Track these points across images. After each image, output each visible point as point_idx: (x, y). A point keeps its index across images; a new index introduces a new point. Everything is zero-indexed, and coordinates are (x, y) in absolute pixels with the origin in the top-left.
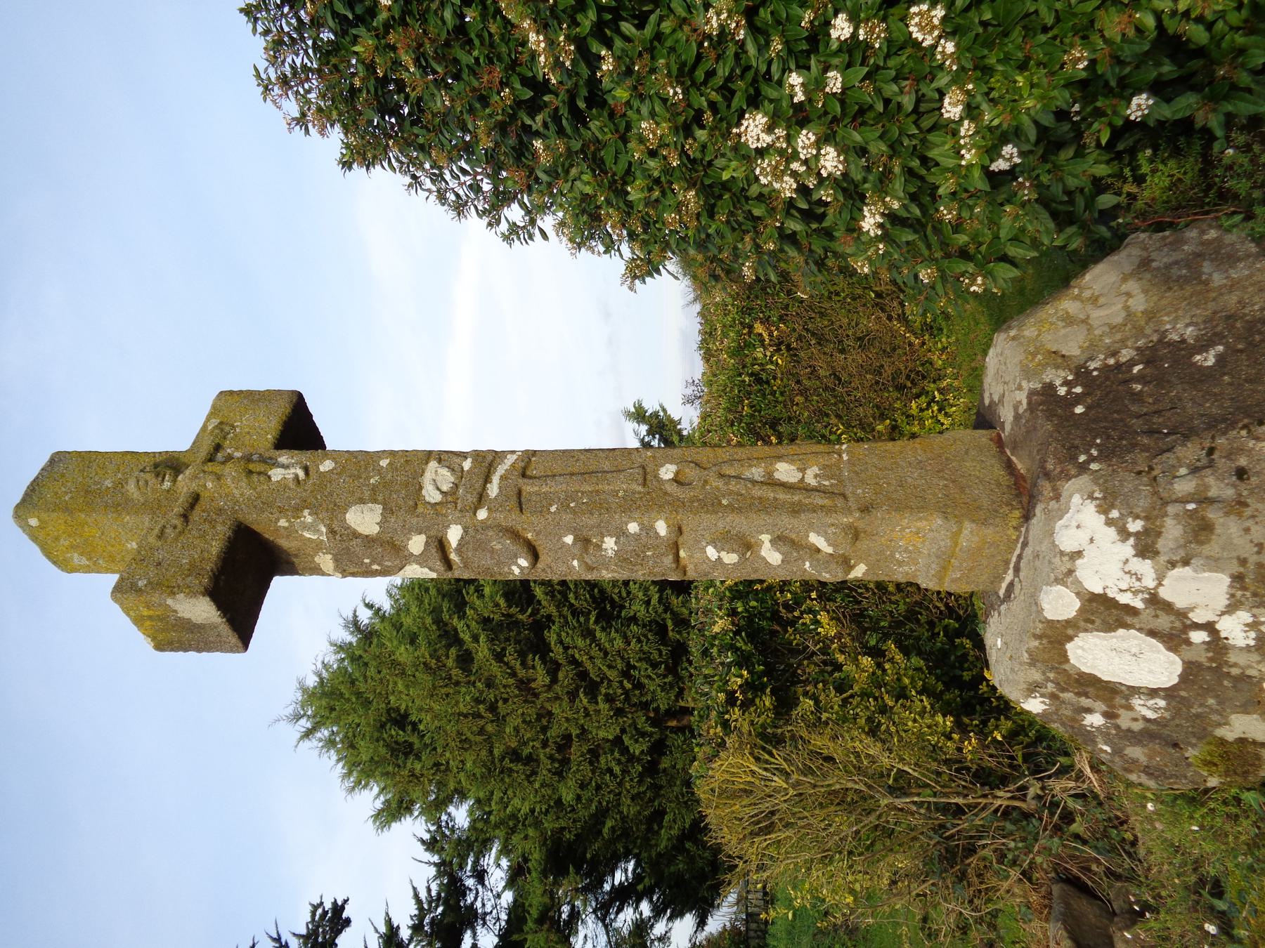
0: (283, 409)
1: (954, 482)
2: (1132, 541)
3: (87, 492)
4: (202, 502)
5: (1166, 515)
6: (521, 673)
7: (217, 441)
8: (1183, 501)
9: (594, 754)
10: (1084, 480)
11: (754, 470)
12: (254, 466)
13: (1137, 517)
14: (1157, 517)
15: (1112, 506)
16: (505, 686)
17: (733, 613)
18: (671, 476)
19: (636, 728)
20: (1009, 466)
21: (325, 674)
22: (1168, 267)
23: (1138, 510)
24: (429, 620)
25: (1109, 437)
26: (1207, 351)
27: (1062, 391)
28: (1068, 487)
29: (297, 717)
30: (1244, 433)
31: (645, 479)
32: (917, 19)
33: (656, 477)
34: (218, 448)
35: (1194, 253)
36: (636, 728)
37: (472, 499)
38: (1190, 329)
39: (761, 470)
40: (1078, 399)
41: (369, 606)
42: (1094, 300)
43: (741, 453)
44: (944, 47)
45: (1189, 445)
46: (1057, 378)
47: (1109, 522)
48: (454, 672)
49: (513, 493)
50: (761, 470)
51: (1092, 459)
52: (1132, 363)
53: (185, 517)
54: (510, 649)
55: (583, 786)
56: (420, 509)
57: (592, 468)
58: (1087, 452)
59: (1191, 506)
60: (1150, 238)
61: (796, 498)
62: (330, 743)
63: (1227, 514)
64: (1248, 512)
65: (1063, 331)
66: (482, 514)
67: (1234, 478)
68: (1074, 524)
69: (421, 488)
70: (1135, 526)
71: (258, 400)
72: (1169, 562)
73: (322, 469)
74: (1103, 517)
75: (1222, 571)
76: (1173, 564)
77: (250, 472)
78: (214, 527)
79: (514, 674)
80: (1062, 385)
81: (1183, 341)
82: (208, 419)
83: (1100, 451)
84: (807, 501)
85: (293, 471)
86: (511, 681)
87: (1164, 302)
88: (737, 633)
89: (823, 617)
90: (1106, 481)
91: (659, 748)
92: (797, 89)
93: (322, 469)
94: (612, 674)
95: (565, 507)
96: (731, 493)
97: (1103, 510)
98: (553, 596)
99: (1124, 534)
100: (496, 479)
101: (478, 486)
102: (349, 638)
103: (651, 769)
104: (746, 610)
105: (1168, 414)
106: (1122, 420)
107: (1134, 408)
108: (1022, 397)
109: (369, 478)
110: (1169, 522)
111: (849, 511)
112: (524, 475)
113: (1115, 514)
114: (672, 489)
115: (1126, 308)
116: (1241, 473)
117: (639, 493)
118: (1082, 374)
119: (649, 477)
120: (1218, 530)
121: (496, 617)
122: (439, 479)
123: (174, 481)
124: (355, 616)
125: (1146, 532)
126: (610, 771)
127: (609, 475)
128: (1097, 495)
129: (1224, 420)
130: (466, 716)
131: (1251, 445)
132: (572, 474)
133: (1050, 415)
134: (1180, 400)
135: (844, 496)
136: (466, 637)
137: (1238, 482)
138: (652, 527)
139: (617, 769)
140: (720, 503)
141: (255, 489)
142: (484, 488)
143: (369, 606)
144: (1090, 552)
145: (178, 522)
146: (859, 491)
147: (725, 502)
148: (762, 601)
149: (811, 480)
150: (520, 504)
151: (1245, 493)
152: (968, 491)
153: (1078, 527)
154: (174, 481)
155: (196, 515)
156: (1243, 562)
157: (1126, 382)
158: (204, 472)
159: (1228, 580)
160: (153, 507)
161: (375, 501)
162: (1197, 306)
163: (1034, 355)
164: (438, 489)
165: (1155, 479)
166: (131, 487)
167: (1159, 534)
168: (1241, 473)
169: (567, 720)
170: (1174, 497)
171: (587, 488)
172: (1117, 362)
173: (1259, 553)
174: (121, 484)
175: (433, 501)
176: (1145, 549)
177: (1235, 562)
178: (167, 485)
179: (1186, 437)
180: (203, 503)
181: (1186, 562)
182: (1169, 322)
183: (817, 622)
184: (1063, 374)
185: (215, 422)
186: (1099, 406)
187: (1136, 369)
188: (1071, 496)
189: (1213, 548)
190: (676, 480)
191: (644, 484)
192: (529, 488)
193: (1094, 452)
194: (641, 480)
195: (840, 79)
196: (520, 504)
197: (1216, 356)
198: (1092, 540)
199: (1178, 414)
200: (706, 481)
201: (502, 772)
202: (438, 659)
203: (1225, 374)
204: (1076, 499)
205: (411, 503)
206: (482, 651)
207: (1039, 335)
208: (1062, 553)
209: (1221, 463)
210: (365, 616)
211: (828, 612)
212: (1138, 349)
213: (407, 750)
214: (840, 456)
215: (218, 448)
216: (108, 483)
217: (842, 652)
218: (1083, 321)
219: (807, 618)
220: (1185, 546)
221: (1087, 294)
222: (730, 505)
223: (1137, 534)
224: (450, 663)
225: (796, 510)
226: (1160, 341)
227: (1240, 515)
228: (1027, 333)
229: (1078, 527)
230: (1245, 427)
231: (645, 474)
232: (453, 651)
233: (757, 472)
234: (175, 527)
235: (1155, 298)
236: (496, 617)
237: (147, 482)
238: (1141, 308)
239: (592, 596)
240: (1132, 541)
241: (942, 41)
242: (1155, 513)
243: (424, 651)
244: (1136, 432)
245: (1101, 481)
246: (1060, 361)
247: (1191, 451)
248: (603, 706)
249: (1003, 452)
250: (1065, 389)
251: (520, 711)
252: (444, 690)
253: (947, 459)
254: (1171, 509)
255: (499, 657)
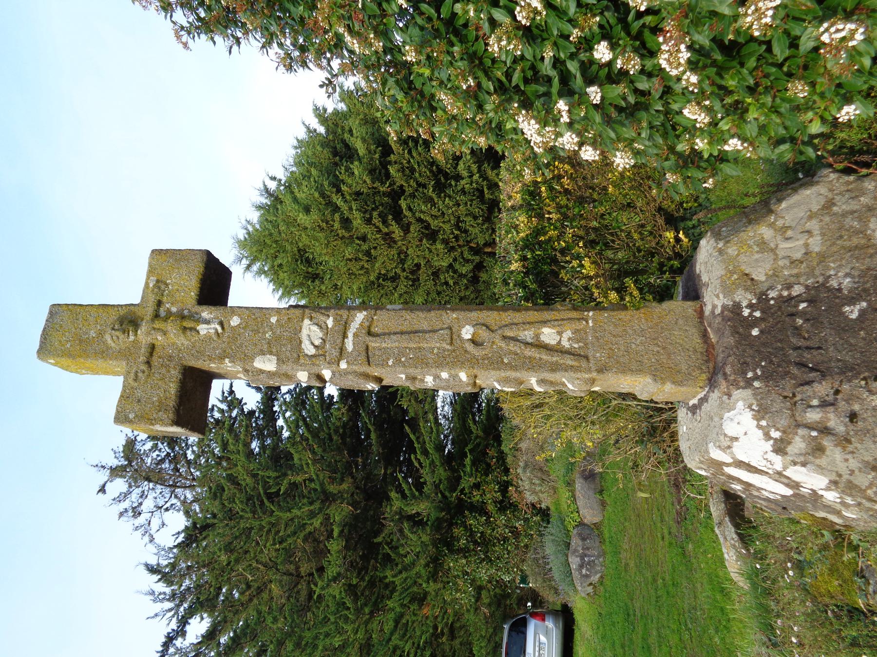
0: (198, 268)
1: (664, 349)
2: (772, 442)
3: (81, 341)
4: (157, 350)
5: (796, 434)
6: (385, 230)
7: (158, 298)
8: (810, 427)
9: (436, 274)
10: (748, 392)
11: (526, 333)
12: (186, 321)
13: (777, 429)
14: (790, 433)
15: (763, 418)
16: (375, 240)
17: (524, 259)
18: (469, 337)
19: (463, 258)
20: (705, 335)
21: (251, 229)
22: (844, 215)
23: (779, 426)
24: (317, 195)
25: (771, 362)
26: (854, 304)
27: (746, 312)
28: (737, 394)
29: (240, 260)
30: (863, 383)
31: (452, 339)
32: (666, 56)
33: (459, 336)
34: (159, 303)
35: (867, 206)
36: (463, 258)
37: (335, 353)
38: (848, 280)
39: (531, 333)
40: (755, 323)
41: (273, 178)
42: (784, 229)
43: (518, 317)
44: (689, 78)
45: (824, 383)
46: (745, 298)
47: (759, 427)
48: (340, 232)
49: (363, 349)
50: (531, 333)
51: (756, 378)
52: (799, 299)
53: (148, 363)
54: (375, 214)
55: (428, 294)
56: (302, 361)
57: (416, 327)
58: (754, 371)
59: (814, 434)
60: (838, 179)
61: (554, 359)
62: (261, 272)
63: (836, 446)
64: (850, 448)
65: (757, 256)
66: (343, 365)
67: (847, 419)
68: (736, 421)
69: (301, 342)
70: (775, 434)
71: (180, 260)
72: (792, 461)
73: (232, 324)
74: (755, 422)
75: (826, 476)
76: (795, 463)
77: (185, 329)
78: (169, 371)
79: (379, 231)
80: (746, 307)
81: (840, 290)
82: (148, 278)
83: (763, 372)
84: (562, 362)
85: (213, 326)
86: (378, 236)
87: (834, 249)
88: (526, 274)
89: (586, 262)
90: (762, 398)
91: (479, 267)
92: (564, 114)
93: (232, 324)
94: (447, 227)
95: (398, 361)
96: (510, 352)
97: (758, 417)
98: (403, 171)
99: (767, 436)
100: (350, 335)
101: (339, 341)
102: (265, 201)
103: (475, 280)
104: (534, 258)
105: (815, 353)
106: (782, 349)
107: (794, 340)
108: (719, 304)
109: (264, 333)
110: (797, 439)
111: (589, 371)
112: (369, 333)
113: (764, 423)
114: (470, 347)
115: (806, 245)
116: (853, 417)
117: (448, 350)
118: (762, 298)
119: (455, 337)
120: (828, 452)
121: (365, 191)
122: (312, 334)
123: (136, 335)
124: (265, 186)
125: (781, 440)
126: (446, 283)
127: (427, 335)
128: (754, 407)
129: (852, 369)
130: (350, 260)
131: (865, 396)
132: (402, 333)
133: (735, 332)
134: (826, 341)
135: (587, 358)
136: (344, 207)
137: (849, 424)
138: (457, 375)
139: (451, 282)
140: (503, 362)
141: (190, 341)
142: (343, 343)
143: (273, 178)
144: (743, 439)
145: (144, 367)
146: (598, 355)
147: (506, 361)
148: (545, 250)
149: (566, 344)
150: (368, 357)
151: (852, 433)
152: (673, 357)
153: (738, 423)
154: (136, 335)
155: (155, 361)
156: (840, 476)
157: (792, 315)
158: (154, 329)
159: (827, 481)
160: (125, 354)
161: (271, 353)
162: (857, 259)
163: (732, 273)
164: (313, 344)
165: (795, 403)
166: (107, 337)
167: (790, 443)
168: (853, 417)
169: (418, 256)
170: (805, 422)
171: (412, 345)
172: (789, 295)
173: (851, 475)
174: (101, 334)
175: (310, 354)
176: (780, 448)
177: (834, 474)
178: (132, 338)
179: (824, 375)
180: (158, 351)
181: (804, 465)
182: (834, 268)
183: (582, 266)
184: (749, 297)
185: (153, 279)
186: (769, 332)
187: (802, 306)
188: (738, 400)
189: (823, 461)
190: (473, 341)
191: (451, 344)
192: (374, 343)
193: (759, 372)
194: (449, 341)
195: (600, 95)
196: (368, 357)
197: (861, 311)
198: (746, 434)
199: (821, 354)
200: (493, 342)
201: (379, 286)
202: (327, 223)
203: (862, 329)
204: (740, 404)
205: (296, 356)
206: (357, 220)
207: (738, 255)
208: (725, 435)
209: (842, 404)
210: (272, 185)
211: (590, 257)
212: (807, 287)
213: (315, 277)
214: (587, 322)
215: (159, 303)
216: (93, 334)
217: (598, 288)
218: (772, 250)
219: (575, 263)
220: (805, 455)
221: (780, 223)
222: (510, 363)
223: (776, 439)
224: (337, 225)
225: (555, 368)
226: (823, 285)
227: (844, 448)
228: (730, 251)
229: (738, 423)
230: (865, 379)
231: (452, 334)
232: (337, 216)
233: (528, 335)
234: (144, 372)
235: (829, 243)
236: (365, 191)
237: (118, 338)
238: (817, 249)
239: (431, 171)
240: (772, 442)
241: (688, 73)
242: (789, 430)
243: (315, 216)
244: (791, 362)
245: (759, 397)
246: (749, 283)
247: (823, 389)
248: (439, 246)
249: (702, 323)
250: (749, 311)
251: (385, 253)
252: (334, 243)
253: (662, 328)
254: (801, 432)
255: (369, 221)
